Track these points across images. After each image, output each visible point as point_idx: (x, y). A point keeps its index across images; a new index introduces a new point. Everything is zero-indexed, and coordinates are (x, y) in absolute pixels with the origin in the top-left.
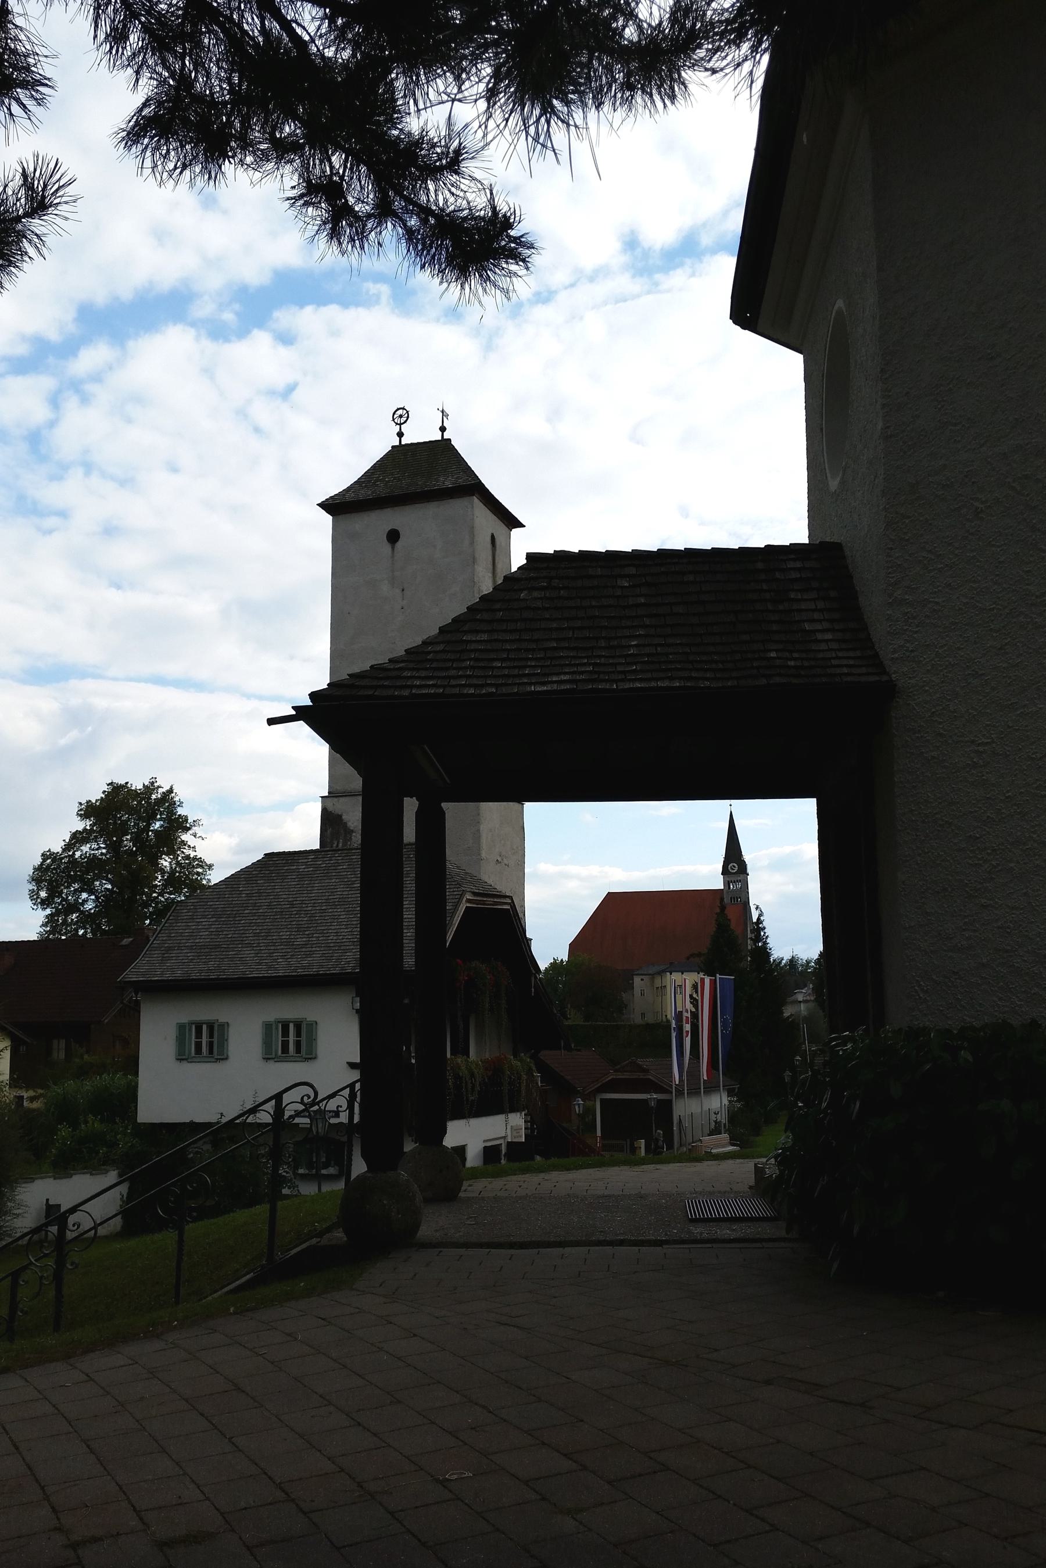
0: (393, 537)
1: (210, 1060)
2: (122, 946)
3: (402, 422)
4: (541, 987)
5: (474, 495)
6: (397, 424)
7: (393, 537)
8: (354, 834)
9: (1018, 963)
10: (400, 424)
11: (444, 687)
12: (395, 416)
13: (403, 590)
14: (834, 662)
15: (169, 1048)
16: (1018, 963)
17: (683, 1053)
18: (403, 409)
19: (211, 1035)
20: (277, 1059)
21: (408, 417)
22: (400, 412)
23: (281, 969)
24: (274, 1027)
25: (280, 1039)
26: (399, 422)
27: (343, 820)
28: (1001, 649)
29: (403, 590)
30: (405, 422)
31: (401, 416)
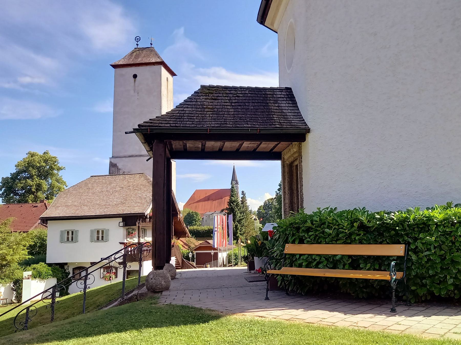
0: (135, 76)
1: (72, 242)
2: (240, 152)
3: (138, 41)
4: (173, 225)
5: (162, 65)
6: (136, 41)
7: (135, 76)
8: (121, 170)
9: (342, 206)
10: (138, 41)
11: (176, 124)
12: (136, 39)
13: (138, 93)
14: (293, 122)
15: (57, 237)
16: (342, 206)
17: (184, 272)
18: (140, 38)
19: (72, 235)
20: (95, 242)
21: (140, 39)
22: (137, 38)
23: (98, 213)
24: (94, 231)
25: (96, 235)
26: (137, 41)
27: (117, 166)
28: (339, 120)
29: (138, 93)
30: (139, 41)
31: (138, 39)
